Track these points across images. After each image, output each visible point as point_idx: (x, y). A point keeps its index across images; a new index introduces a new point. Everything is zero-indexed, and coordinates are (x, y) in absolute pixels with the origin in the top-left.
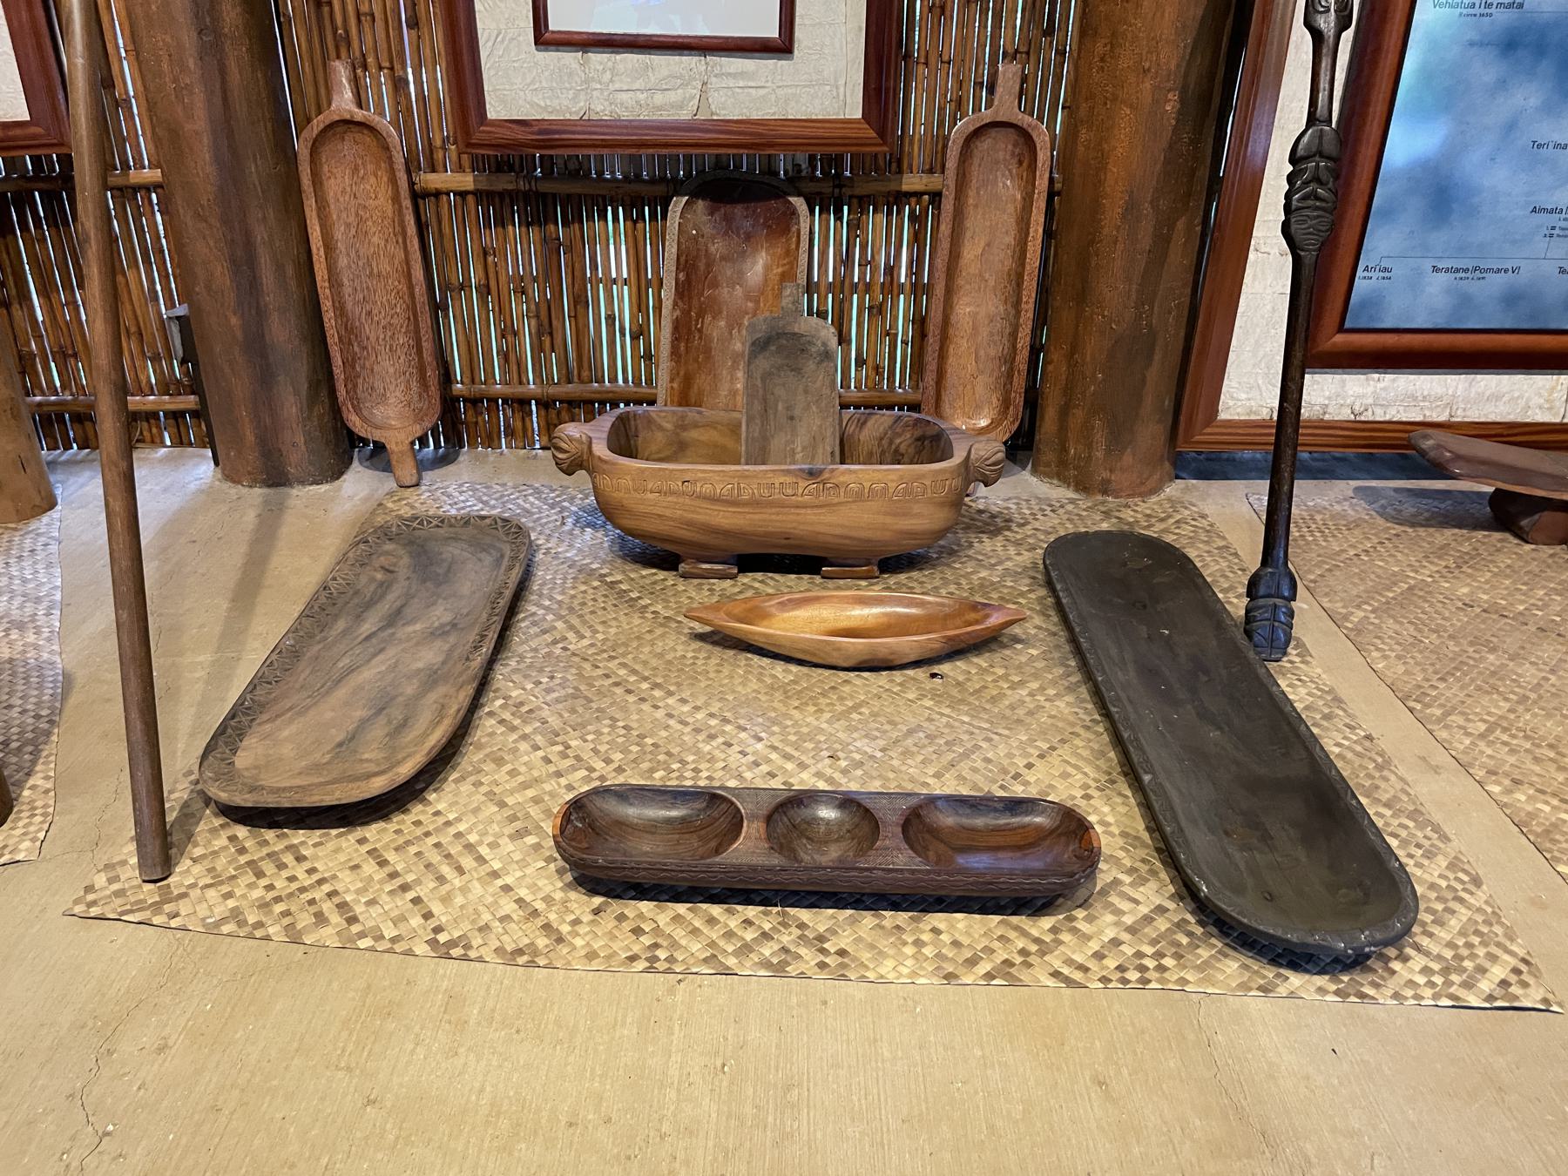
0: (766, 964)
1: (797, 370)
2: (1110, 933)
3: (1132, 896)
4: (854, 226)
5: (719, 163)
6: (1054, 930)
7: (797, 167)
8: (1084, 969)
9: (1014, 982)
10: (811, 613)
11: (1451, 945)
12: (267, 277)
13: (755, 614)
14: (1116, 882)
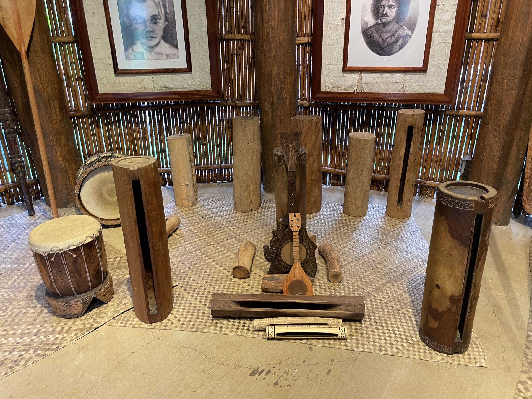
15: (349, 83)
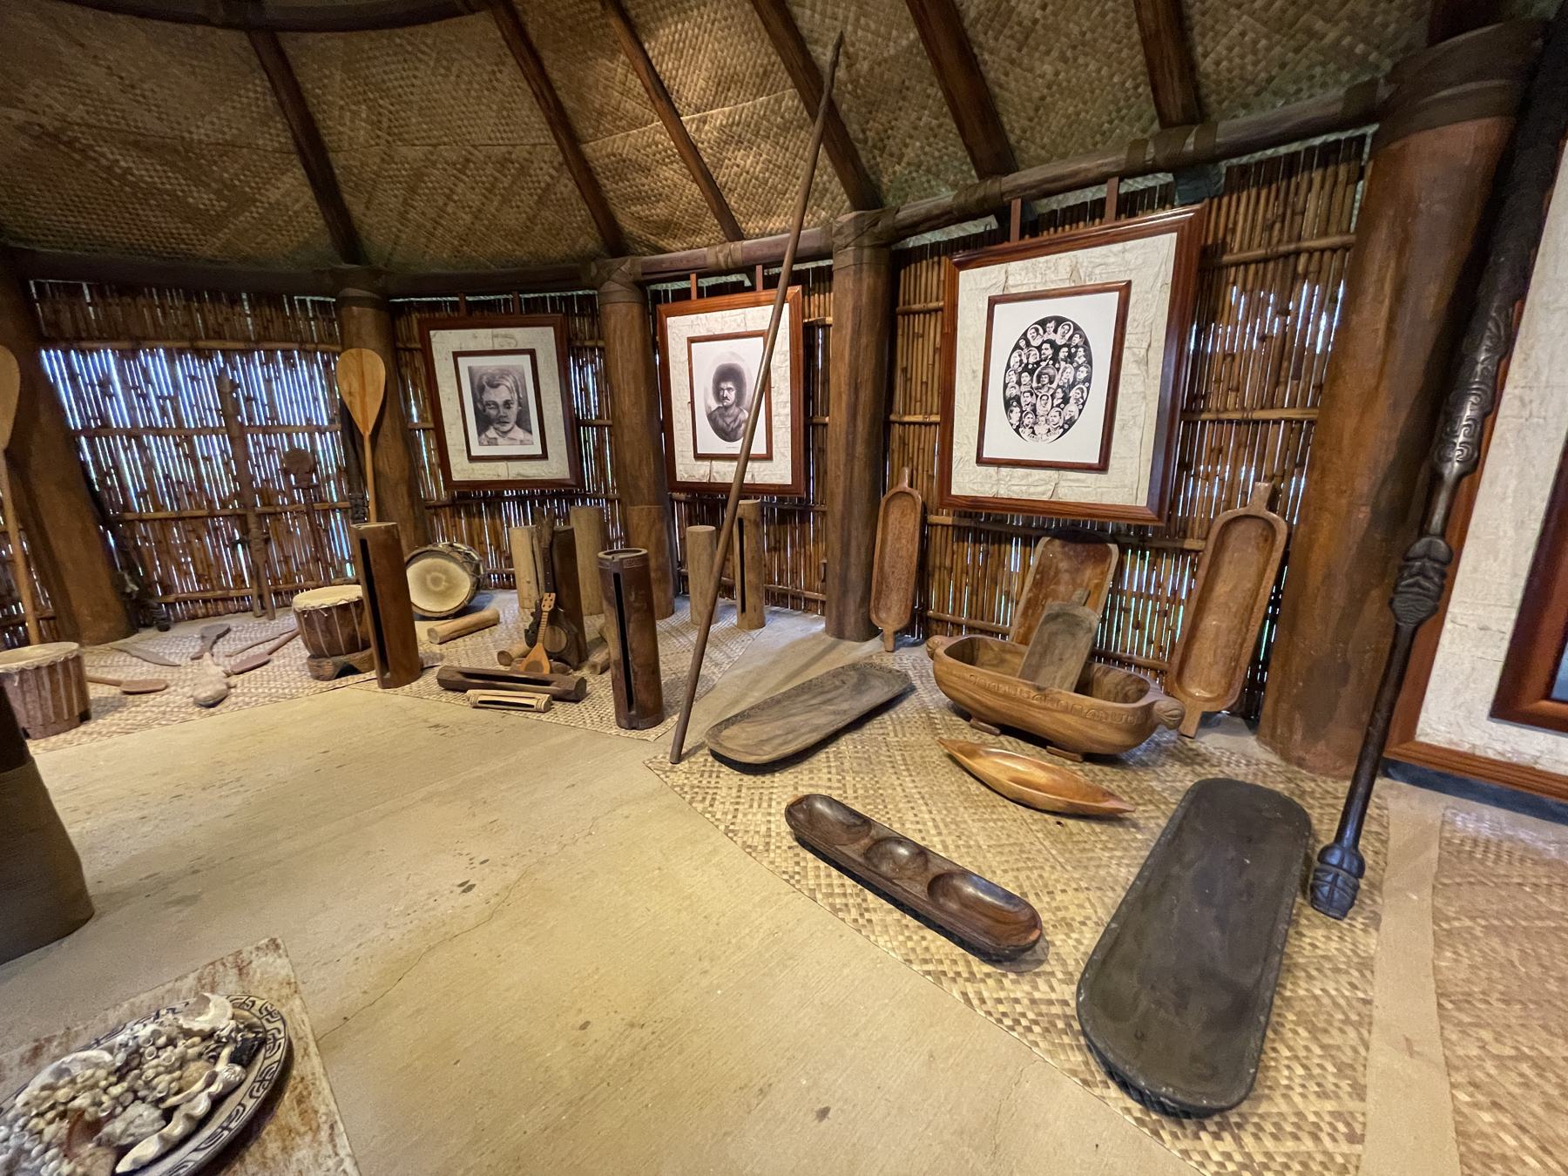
0: (832, 906)
1: (1073, 635)
2: (1019, 995)
3: (1056, 986)
4: (1152, 565)
5: (1075, 524)
6: (988, 975)
7: (1119, 529)
8: (983, 1001)
9: (938, 981)
10: (1014, 763)
11: (1268, 1155)
12: (853, 551)
13: (972, 753)
14: (1052, 974)
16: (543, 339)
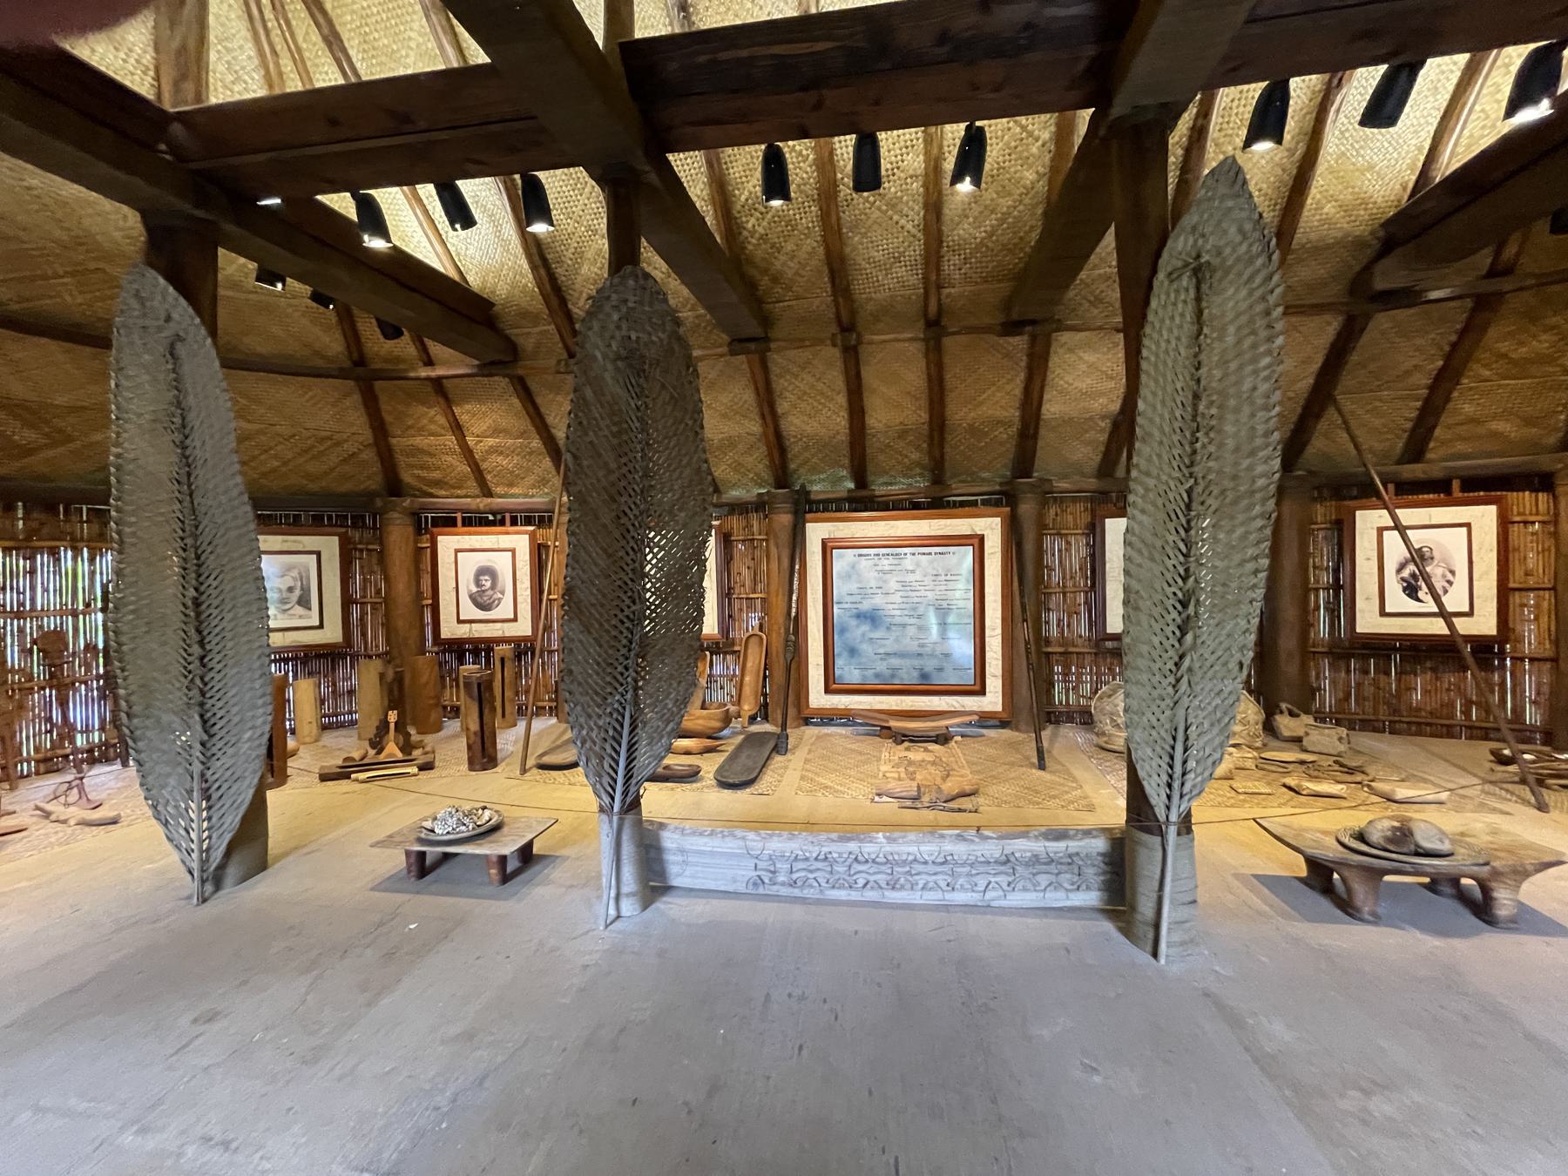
15: (463, 631)
16: (330, 545)
